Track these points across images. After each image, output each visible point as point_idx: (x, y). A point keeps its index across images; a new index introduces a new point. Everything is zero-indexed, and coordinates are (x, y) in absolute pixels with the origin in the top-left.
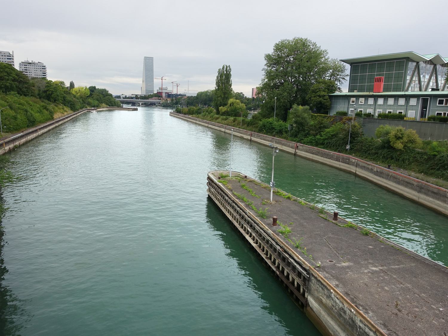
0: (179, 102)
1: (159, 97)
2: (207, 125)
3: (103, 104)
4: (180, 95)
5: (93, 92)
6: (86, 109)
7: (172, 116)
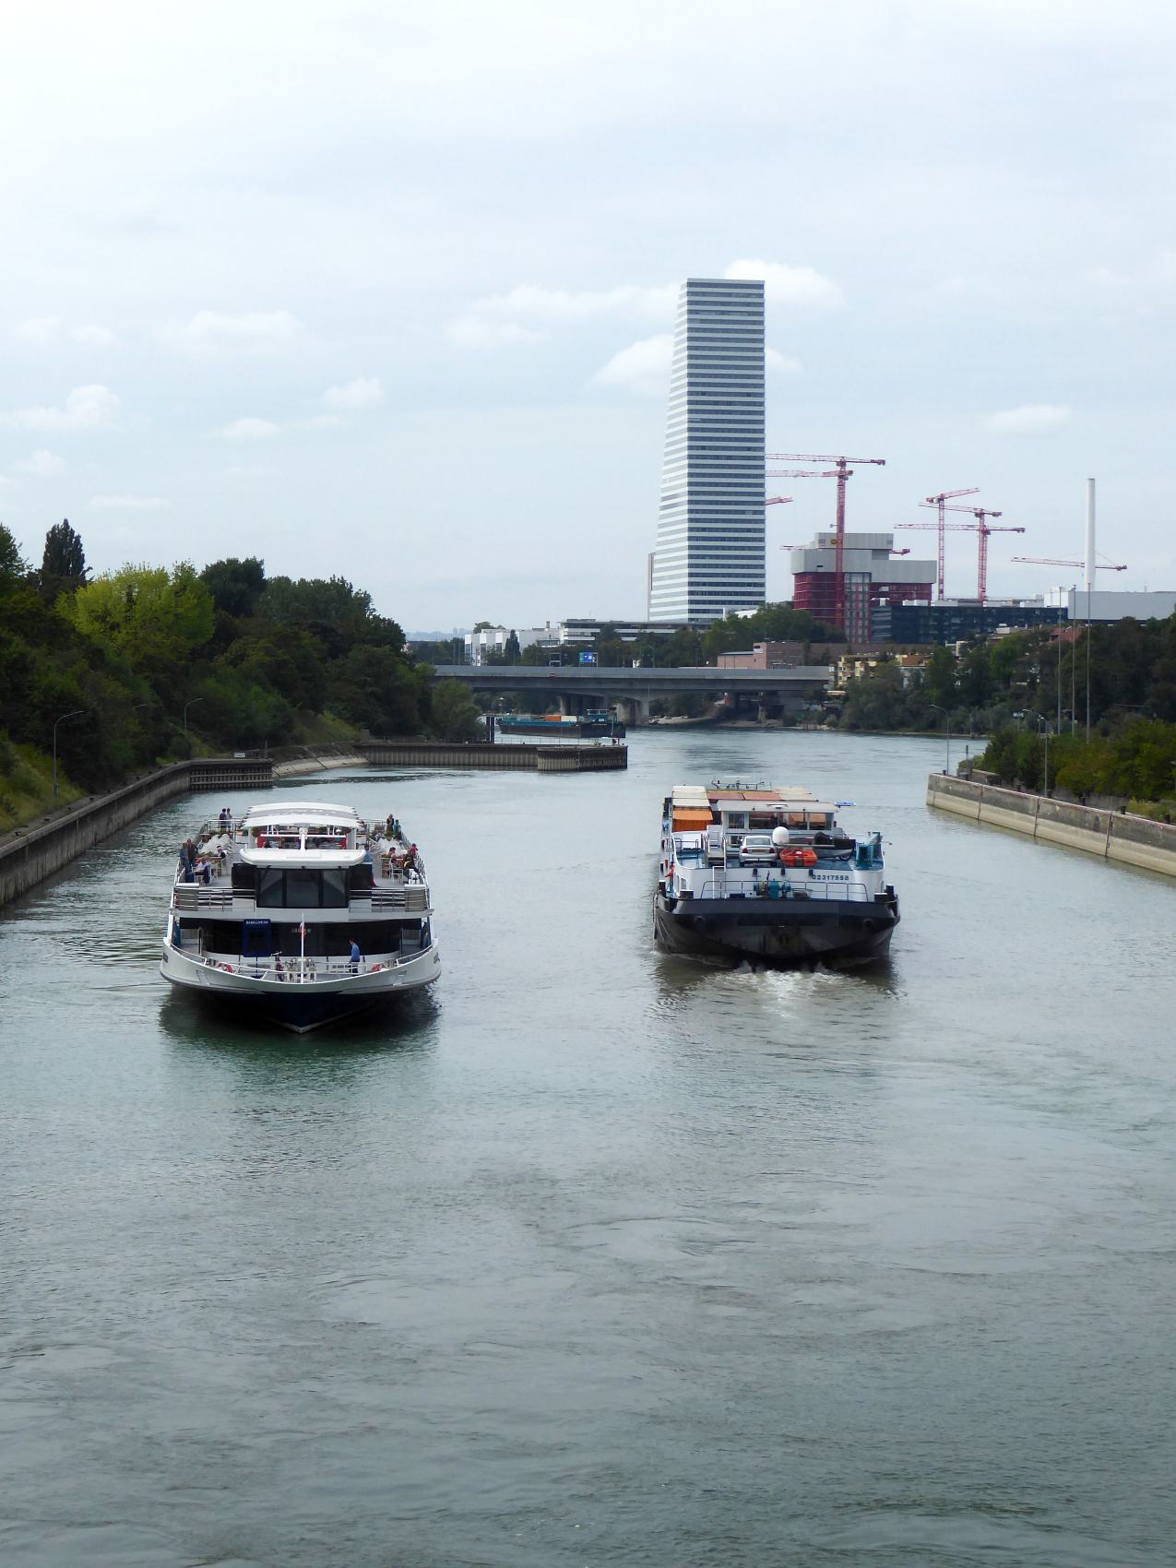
0: (1007, 679)
1: (817, 635)
2: (1096, 842)
3: (327, 718)
4: (1011, 614)
5: (887, 661)
6: (181, 764)
7: (950, 814)
